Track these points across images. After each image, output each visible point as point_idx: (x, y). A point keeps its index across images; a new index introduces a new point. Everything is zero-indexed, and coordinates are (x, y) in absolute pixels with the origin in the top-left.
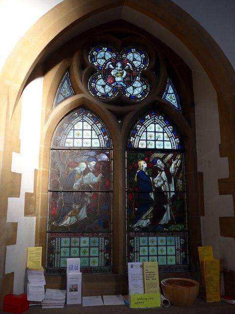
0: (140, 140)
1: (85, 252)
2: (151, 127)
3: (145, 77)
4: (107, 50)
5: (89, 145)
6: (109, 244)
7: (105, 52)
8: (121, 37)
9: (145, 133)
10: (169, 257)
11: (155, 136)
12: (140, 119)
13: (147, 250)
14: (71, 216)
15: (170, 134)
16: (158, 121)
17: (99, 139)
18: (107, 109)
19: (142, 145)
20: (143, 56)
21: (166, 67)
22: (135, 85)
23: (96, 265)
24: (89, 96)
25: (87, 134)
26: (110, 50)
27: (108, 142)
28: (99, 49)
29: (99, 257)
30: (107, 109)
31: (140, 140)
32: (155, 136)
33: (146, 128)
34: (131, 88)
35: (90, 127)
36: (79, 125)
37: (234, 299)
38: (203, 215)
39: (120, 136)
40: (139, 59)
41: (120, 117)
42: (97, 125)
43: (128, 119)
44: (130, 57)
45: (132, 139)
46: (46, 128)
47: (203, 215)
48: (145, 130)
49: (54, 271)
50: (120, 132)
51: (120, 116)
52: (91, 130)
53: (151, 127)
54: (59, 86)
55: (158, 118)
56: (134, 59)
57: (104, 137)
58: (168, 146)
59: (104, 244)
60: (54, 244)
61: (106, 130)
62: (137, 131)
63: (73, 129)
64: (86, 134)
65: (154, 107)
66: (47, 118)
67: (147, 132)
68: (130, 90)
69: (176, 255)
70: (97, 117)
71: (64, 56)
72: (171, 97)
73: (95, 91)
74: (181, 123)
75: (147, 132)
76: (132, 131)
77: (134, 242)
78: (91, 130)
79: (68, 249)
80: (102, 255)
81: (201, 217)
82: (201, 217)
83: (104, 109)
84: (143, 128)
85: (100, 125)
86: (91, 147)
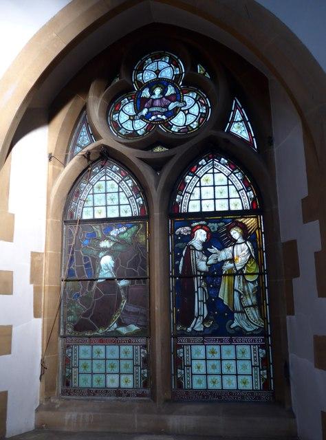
0: (190, 200)
1: (99, 366)
6: (148, 355)
9: (197, 190)
11: (215, 189)
12: (189, 166)
13: (110, 362)
15: (240, 185)
18: (141, 159)
19: (194, 207)
23: (130, 385)
24: (107, 139)
25: (222, 192)
27: (254, 200)
28: (157, 58)
29: (252, 375)
30: (141, 159)
31: (190, 200)
32: (215, 189)
33: (200, 181)
38: (291, 312)
41: (163, 165)
42: (237, 175)
43: (167, 170)
47: (291, 312)
48: (91, 192)
51: (157, 165)
53: (207, 179)
55: (219, 162)
57: (137, 200)
58: (236, 205)
59: (259, 356)
60: (181, 355)
61: (141, 189)
62: (185, 184)
64: (111, 197)
65: (210, 144)
66: (55, 174)
67: (200, 187)
69: (192, 374)
70: (127, 168)
72: (239, 130)
74: (252, 166)
75: (200, 187)
76: (175, 186)
77: (72, 353)
78: (228, 185)
79: (233, 363)
80: (256, 374)
81: (288, 317)
82: (288, 317)
83: (131, 158)
85: (239, 176)
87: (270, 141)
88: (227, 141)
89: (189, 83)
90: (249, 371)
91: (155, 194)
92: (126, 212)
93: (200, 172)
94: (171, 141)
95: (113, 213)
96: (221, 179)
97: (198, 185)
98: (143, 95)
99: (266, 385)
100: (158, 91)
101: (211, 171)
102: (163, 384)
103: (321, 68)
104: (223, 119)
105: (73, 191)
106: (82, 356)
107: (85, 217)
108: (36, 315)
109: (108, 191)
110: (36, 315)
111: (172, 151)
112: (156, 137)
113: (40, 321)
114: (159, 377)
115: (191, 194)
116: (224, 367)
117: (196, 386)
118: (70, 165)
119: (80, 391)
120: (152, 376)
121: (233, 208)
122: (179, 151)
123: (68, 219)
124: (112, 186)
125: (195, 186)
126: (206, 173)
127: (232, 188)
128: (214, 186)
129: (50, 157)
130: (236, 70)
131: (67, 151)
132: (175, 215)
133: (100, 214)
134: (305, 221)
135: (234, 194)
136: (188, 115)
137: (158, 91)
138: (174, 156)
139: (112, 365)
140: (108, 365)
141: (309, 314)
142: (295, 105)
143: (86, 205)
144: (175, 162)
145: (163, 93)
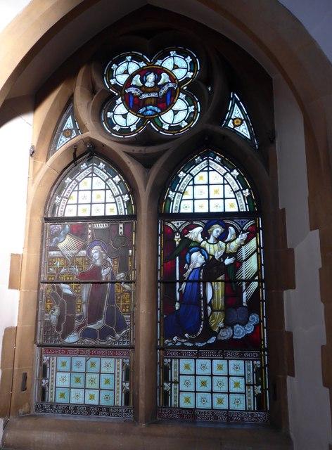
0: (182, 200)
2: (201, 178)
3: (193, 90)
4: (132, 59)
7: (114, 114)
8: (152, 38)
10: (232, 372)
16: (213, 165)
17: (115, 202)
19: (186, 208)
20: (189, 59)
21: (231, 70)
22: (176, 107)
24: (92, 133)
25: (216, 191)
26: (136, 59)
31: (182, 200)
32: (210, 189)
33: (193, 180)
34: (170, 113)
35: (220, 180)
36: (86, 184)
40: (184, 65)
41: (156, 162)
43: (158, 166)
44: (168, 64)
48: (76, 189)
52: (105, 190)
53: (201, 178)
56: (176, 67)
61: (130, 186)
63: (107, 188)
64: (96, 195)
65: (206, 141)
66: (35, 175)
68: (167, 117)
70: (115, 165)
71: (59, 67)
72: (238, 120)
73: (111, 124)
74: (253, 165)
76: (168, 181)
78: (224, 184)
84: (188, 178)
86: (195, 359)
87: (272, 139)
88: (224, 137)
90: (241, 388)
91: (144, 194)
92: (112, 211)
93: (194, 171)
96: (215, 178)
97: (191, 183)
99: (260, 399)
100: (151, 77)
101: (206, 169)
102: (150, 403)
104: (220, 114)
105: (57, 186)
106: (59, 384)
107: (68, 215)
108: (12, 285)
110: (12, 285)
112: (148, 137)
113: (16, 295)
114: (142, 393)
115: (183, 194)
116: (214, 384)
117: (183, 405)
118: (52, 159)
119: (54, 407)
120: (134, 385)
121: (228, 210)
123: (49, 216)
124: (98, 183)
125: (188, 185)
126: (202, 170)
127: (227, 187)
128: (209, 199)
129: (32, 154)
131: (54, 184)
132: (162, 213)
134: (311, 230)
135: (229, 194)
137: (151, 77)
138: (167, 150)
139: (88, 381)
140: (88, 380)
141: (303, 311)
142: (292, 83)
143: (70, 202)
144: (168, 156)
145: (157, 80)
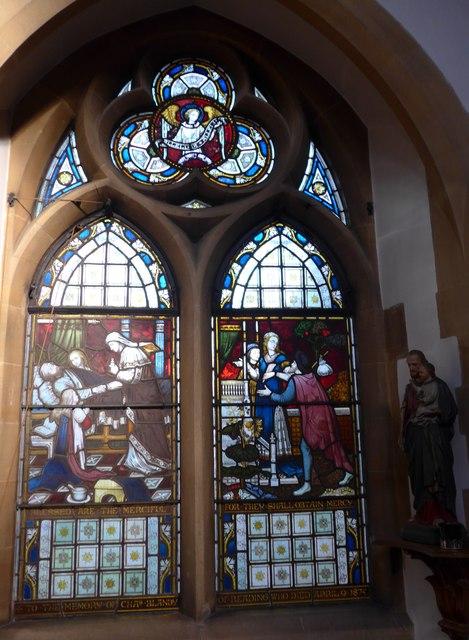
5: (83, 524)
12: (248, 229)
14: (114, 378)
25: (117, 275)
32: (278, 274)
37: (450, 617)
39: (195, 280)
41: (197, 230)
43: (212, 239)
45: (226, 293)
46: (14, 263)
49: (144, 606)
50: (196, 268)
51: (194, 230)
54: (38, 195)
64: (113, 271)
65: (273, 204)
66: (17, 240)
70: (138, 225)
74: (339, 246)
76: (218, 278)
83: (154, 213)
89: (246, 114)
94: (219, 195)
95: (116, 300)
98: (322, 362)
101: (310, 283)
103: (460, 104)
109: (66, 280)
111: (219, 211)
112: (194, 179)
122: (235, 210)
129: (12, 200)
130: (321, 100)
133: (93, 299)
136: (247, 159)
